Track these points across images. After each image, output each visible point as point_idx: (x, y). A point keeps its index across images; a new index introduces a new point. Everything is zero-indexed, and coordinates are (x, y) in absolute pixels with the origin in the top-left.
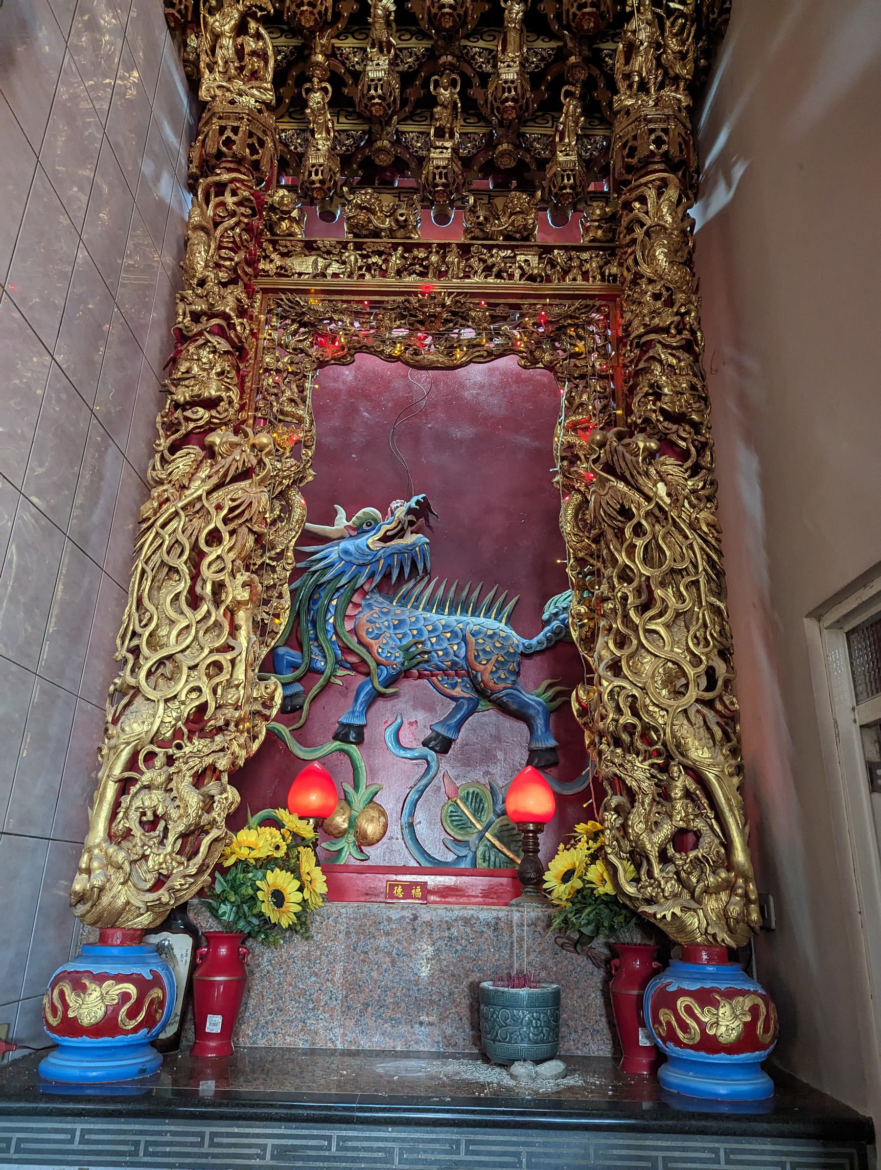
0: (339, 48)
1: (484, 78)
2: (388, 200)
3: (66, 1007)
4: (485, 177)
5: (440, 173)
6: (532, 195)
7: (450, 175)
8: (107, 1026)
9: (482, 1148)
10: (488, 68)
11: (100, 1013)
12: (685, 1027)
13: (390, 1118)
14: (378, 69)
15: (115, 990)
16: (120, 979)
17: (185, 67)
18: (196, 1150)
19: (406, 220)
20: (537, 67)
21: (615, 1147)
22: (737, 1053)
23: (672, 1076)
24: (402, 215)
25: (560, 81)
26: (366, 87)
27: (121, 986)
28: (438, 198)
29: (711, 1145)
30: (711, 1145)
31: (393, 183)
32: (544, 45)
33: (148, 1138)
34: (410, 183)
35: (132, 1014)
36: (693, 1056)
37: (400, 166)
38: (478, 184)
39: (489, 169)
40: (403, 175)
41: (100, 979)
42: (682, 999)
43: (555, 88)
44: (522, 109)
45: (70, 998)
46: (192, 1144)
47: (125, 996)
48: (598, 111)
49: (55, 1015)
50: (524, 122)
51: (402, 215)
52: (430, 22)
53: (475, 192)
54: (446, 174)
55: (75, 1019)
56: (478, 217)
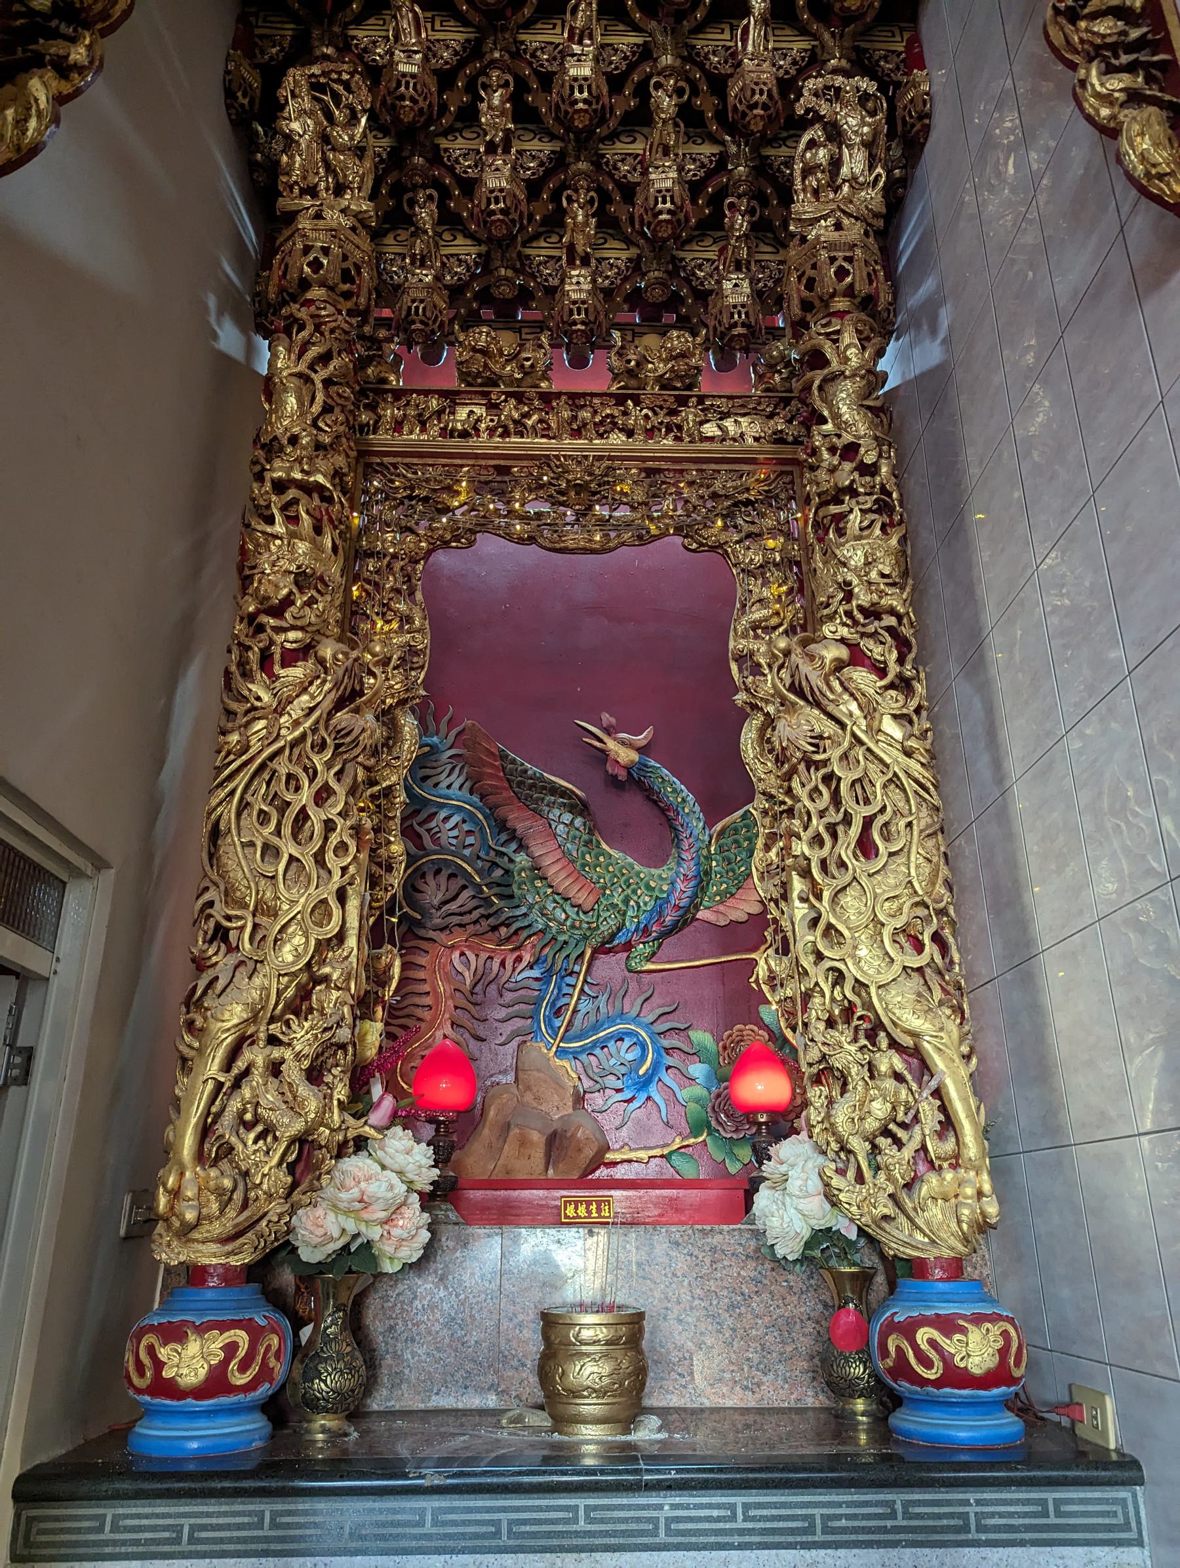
0: (446, 150)
1: (629, 192)
2: (507, 341)
3: (159, 1365)
4: (632, 310)
5: (579, 310)
6: (694, 335)
7: (591, 310)
8: (216, 1383)
9: (775, 1512)
10: (635, 177)
11: (203, 1373)
12: (928, 1363)
13: (571, 1483)
14: (497, 178)
15: (216, 1343)
16: (223, 1327)
17: (251, 173)
18: (728, 1526)
19: (532, 366)
20: (616, 68)
21: (452, 1510)
22: (959, 1388)
23: (906, 1420)
24: (528, 359)
25: (722, 193)
26: (484, 201)
27: (227, 1334)
28: (582, 343)
29: (724, 1500)
30: (724, 1500)
31: (516, 316)
32: (627, 41)
33: (192, 1521)
34: (535, 315)
35: (244, 1367)
36: (917, 1393)
37: (524, 297)
38: (623, 317)
39: (635, 299)
40: (527, 307)
41: (201, 1330)
42: (926, 1329)
43: (716, 201)
44: (677, 223)
45: (163, 1353)
46: (204, 1528)
47: (230, 1349)
48: (772, 229)
49: (142, 1374)
50: (683, 244)
51: (528, 359)
52: (557, 119)
53: (620, 327)
54: (586, 310)
55: (172, 1380)
56: (629, 361)
